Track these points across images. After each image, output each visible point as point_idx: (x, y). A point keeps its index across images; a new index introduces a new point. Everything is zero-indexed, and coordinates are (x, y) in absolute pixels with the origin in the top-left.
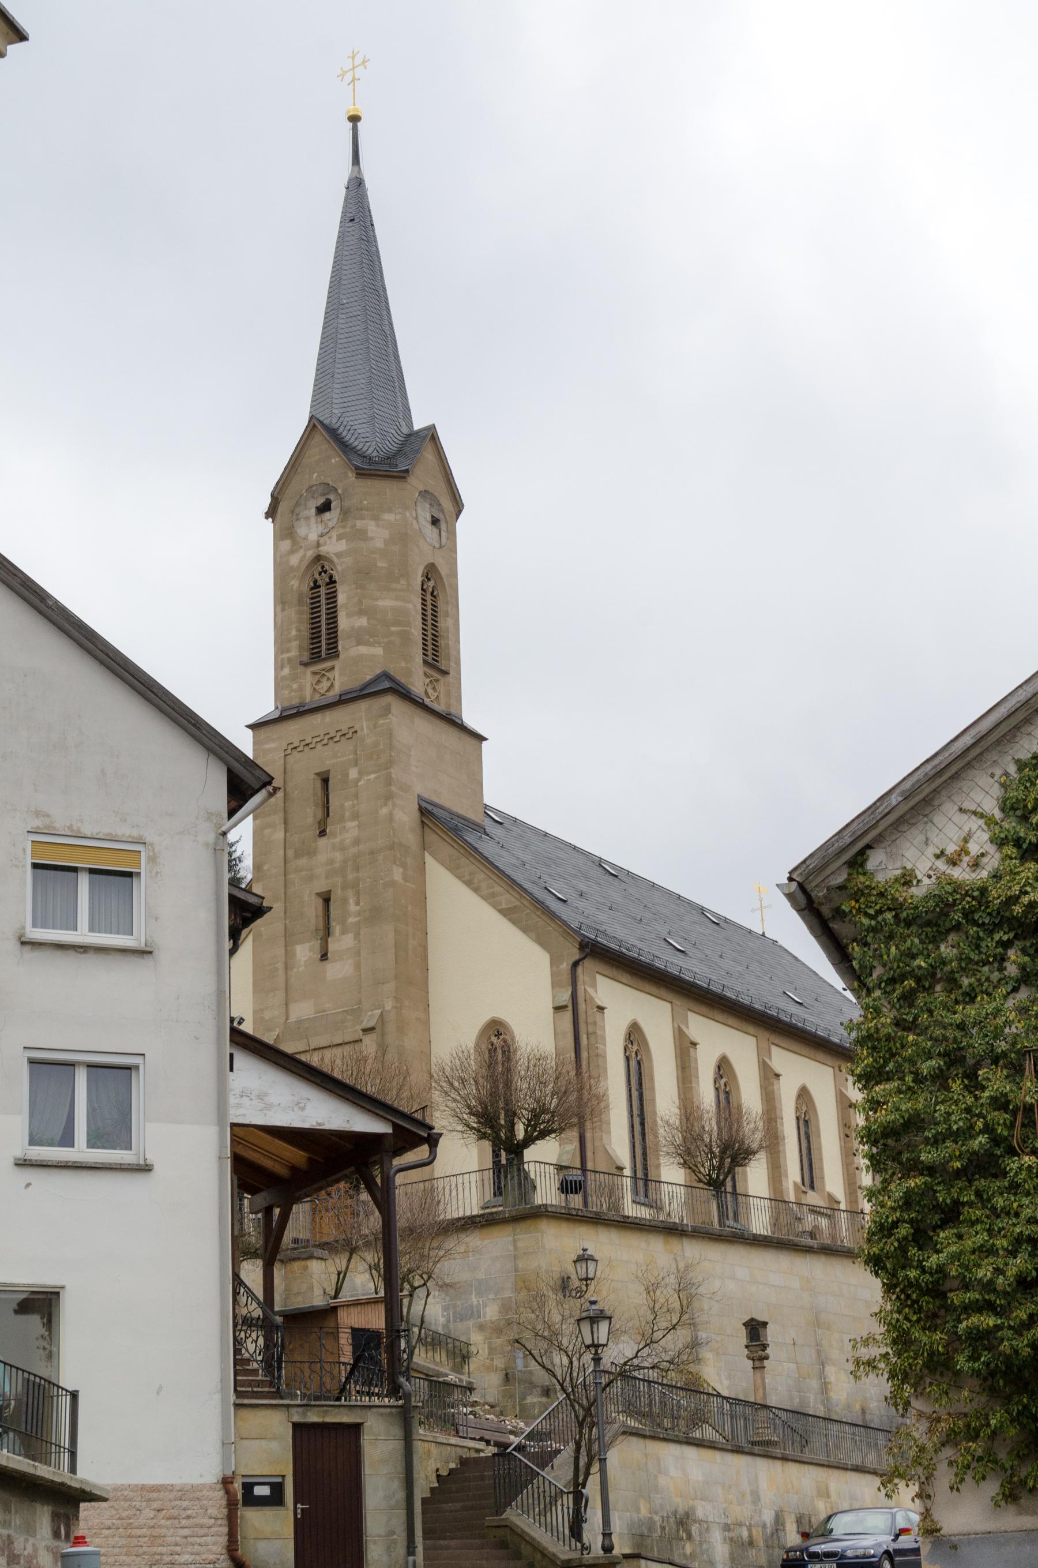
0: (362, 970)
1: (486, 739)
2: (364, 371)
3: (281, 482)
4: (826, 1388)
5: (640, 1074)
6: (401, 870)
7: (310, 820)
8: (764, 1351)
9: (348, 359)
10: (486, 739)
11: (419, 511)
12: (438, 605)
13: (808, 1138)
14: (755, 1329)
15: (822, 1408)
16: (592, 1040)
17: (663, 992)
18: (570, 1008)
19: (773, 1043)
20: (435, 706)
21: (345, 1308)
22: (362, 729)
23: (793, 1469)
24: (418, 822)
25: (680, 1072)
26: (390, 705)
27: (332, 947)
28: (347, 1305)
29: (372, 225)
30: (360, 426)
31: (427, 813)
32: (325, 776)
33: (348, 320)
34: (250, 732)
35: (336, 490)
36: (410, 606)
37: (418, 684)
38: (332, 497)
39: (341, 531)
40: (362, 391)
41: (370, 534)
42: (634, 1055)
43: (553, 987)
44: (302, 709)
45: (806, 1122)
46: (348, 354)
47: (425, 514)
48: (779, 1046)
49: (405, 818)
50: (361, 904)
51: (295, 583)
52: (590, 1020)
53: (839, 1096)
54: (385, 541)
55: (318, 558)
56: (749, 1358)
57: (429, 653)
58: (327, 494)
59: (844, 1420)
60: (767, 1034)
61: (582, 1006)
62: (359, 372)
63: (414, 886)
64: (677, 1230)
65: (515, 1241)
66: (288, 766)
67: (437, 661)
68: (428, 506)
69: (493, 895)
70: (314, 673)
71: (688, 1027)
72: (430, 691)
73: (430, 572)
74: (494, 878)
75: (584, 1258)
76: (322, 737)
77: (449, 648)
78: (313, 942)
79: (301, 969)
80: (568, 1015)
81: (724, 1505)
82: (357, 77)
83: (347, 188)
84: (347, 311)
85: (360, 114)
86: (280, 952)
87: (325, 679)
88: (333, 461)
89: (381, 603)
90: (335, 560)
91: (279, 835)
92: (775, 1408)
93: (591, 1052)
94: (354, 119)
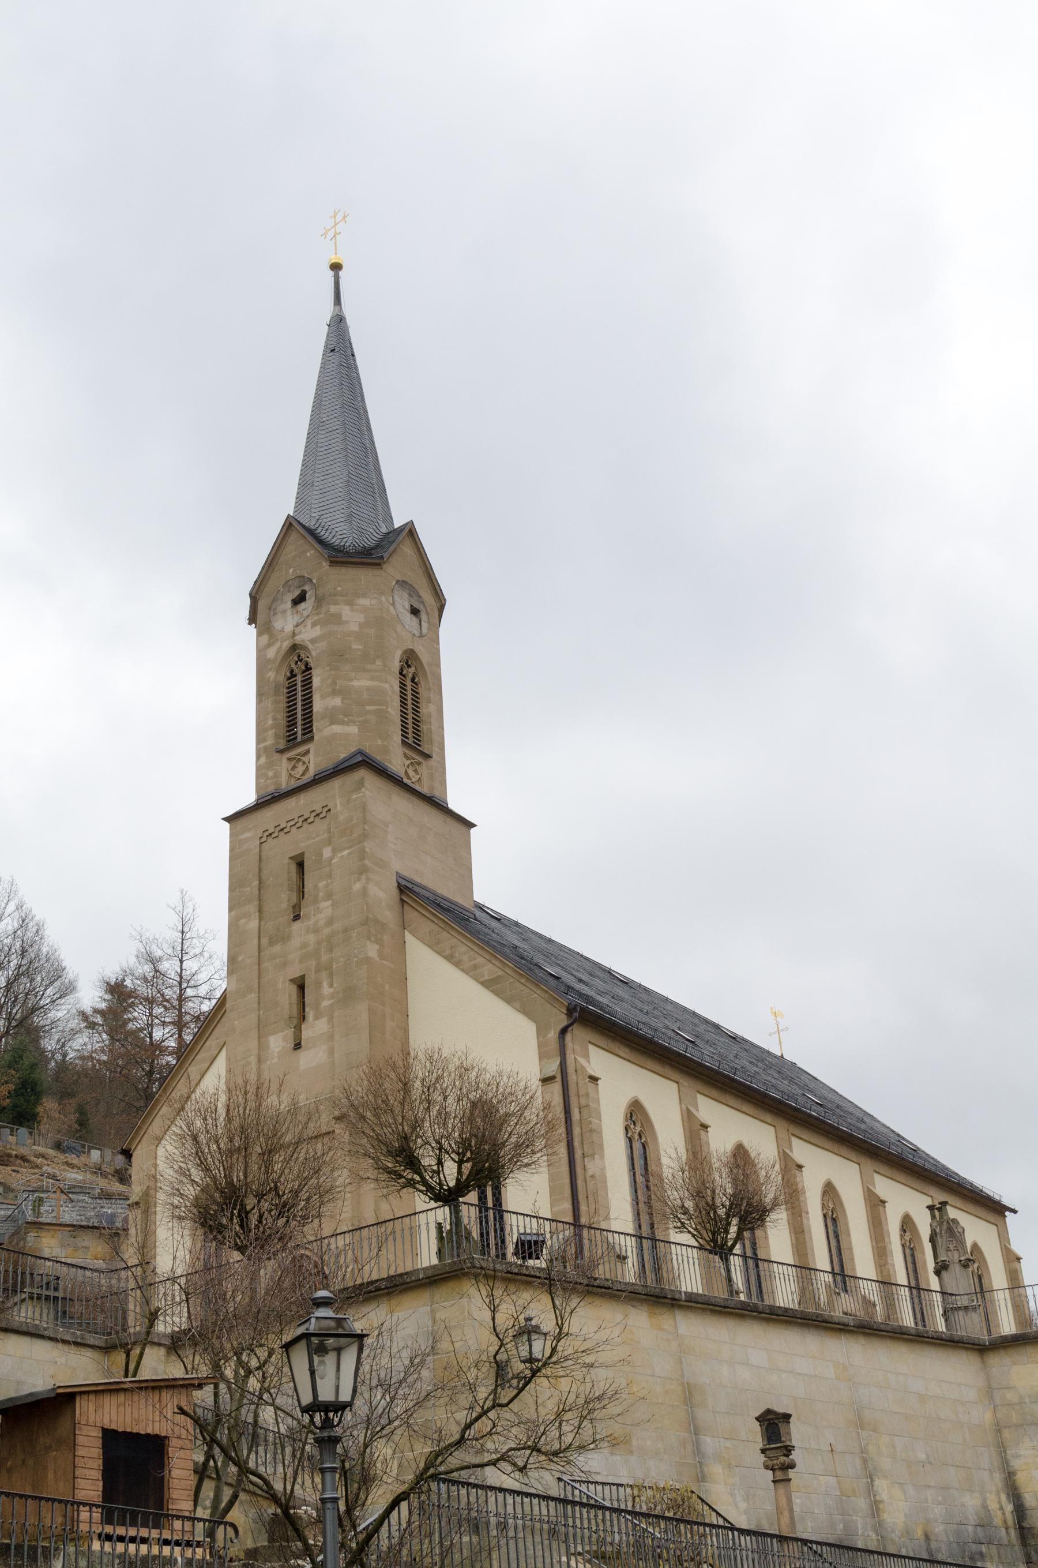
0: (336, 1056)
1: (473, 825)
2: (342, 476)
3: (259, 582)
4: (878, 1509)
6: (377, 947)
7: (284, 905)
8: (787, 1456)
9: (327, 468)
11: (396, 598)
12: (420, 692)
13: (837, 1237)
15: (874, 1536)
16: (585, 1112)
17: (668, 1071)
20: (417, 787)
21: (92, 1397)
22: (336, 806)
24: (398, 899)
26: (363, 778)
27: (305, 1034)
28: (96, 1392)
29: (353, 355)
30: (337, 525)
32: (299, 860)
33: (327, 435)
34: (227, 825)
35: (311, 580)
36: (387, 686)
37: (397, 761)
38: (306, 588)
39: (316, 618)
40: (340, 494)
41: (344, 619)
42: (636, 1137)
43: (541, 1058)
45: (834, 1220)
46: (327, 464)
47: (402, 602)
48: (801, 1139)
49: (381, 894)
50: (335, 985)
51: (271, 675)
52: (582, 1093)
53: (866, 1194)
54: (360, 625)
55: (294, 647)
56: (766, 1467)
57: (410, 736)
58: (303, 585)
59: (904, 1553)
61: (572, 1078)
62: (338, 478)
63: (392, 966)
64: (666, 1298)
65: (433, 1312)
66: (264, 854)
67: (419, 745)
68: (406, 595)
69: (475, 967)
70: (290, 759)
71: (698, 1110)
72: (411, 773)
73: (409, 659)
74: (475, 948)
77: (431, 733)
78: (286, 1032)
79: (274, 1061)
80: (556, 1087)
82: (338, 232)
84: (327, 427)
86: (253, 1044)
87: (301, 763)
88: (308, 554)
89: (355, 683)
90: (310, 646)
91: (254, 924)
93: (584, 1127)
94: (336, 267)
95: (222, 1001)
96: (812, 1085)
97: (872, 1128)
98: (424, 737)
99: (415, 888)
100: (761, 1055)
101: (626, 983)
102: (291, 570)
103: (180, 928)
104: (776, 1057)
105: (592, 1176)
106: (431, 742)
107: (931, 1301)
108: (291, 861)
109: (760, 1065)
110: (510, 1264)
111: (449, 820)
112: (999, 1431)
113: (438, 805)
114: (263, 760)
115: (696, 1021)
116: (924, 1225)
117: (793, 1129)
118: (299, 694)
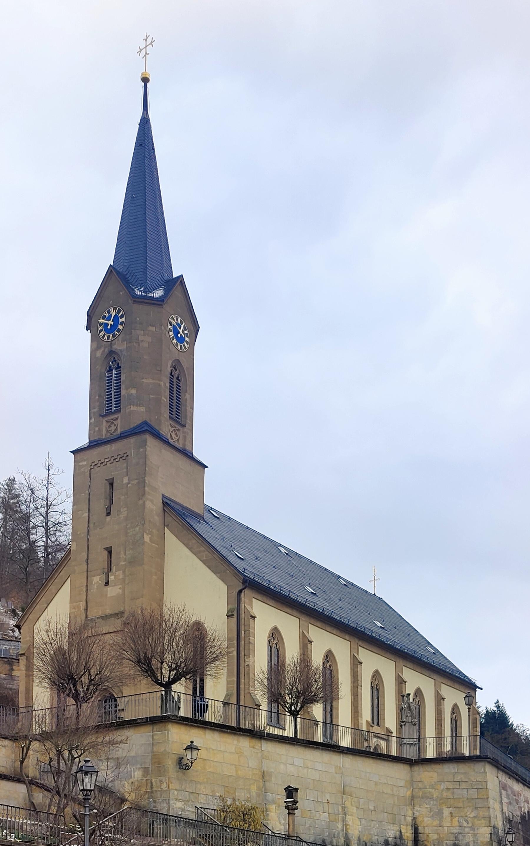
1: (207, 467)
2: (143, 239)
10: (207, 467)
14: (291, 792)
19: (360, 646)
20: (176, 444)
24: (161, 509)
27: (112, 578)
30: (139, 274)
32: (111, 481)
33: (135, 208)
40: (141, 252)
42: (274, 645)
44: (100, 442)
48: (364, 648)
60: (357, 640)
61: (243, 615)
63: (157, 546)
67: (179, 419)
72: (173, 435)
73: (177, 366)
74: (200, 542)
75: (191, 747)
79: (94, 590)
80: (235, 619)
83: (139, 125)
85: (148, 76)
87: (113, 425)
88: (121, 293)
90: (120, 353)
94: (145, 80)
99: (172, 504)
102: (111, 302)
104: (370, 594)
105: (248, 665)
108: (106, 482)
111: (193, 464)
113: (188, 455)
114: (93, 420)
117: (360, 643)
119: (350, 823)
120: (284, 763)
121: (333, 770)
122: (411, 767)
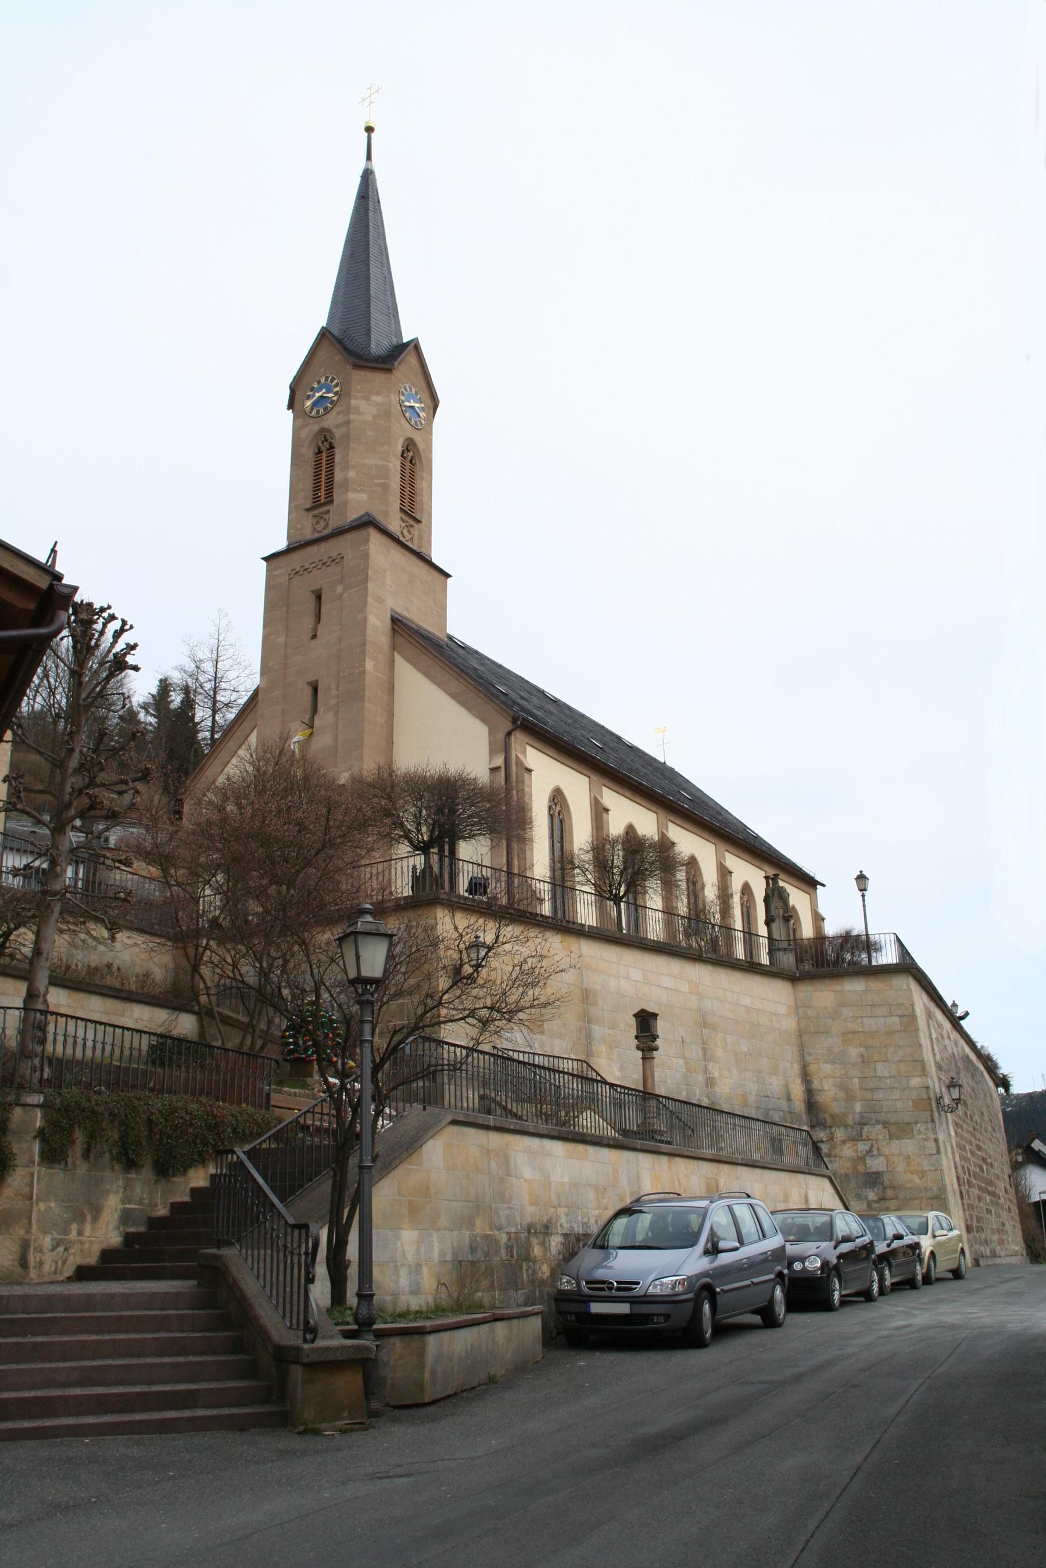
5: (562, 830)
14: (645, 1021)
18: (503, 769)
20: (409, 544)
23: (680, 1164)
25: (594, 831)
31: (398, 624)
34: (265, 563)
37: (395, 525)
42: (557, 815)
48: (675, 823)
49: (379, 623)
50: (341, 689)
51: (304, 450)
56: (638, 1048)
61: (514, 768)
73: (410, 445)
76: (317, 563)
81: (597, 1212)
90: (334, 430)
92: (663, 1097)
94: (369, 130)
95: (256, 693)
96: (685, 785)
97: (726, 819)
98: (417, 507)
100: (649, 761)
101: (556, 702)
103: (216, 637)
104: (659, 762)
106: (422, 510)
107: (758, 944)
109: (649, 768)
110: (460, 897)
112: (800, 1036)
115: (604, 733)
116: (759, 891)
118: (324, 467)
119: (716, 1075)
120: (615, 976)
121: (685, 987)
122: (793, 984)
